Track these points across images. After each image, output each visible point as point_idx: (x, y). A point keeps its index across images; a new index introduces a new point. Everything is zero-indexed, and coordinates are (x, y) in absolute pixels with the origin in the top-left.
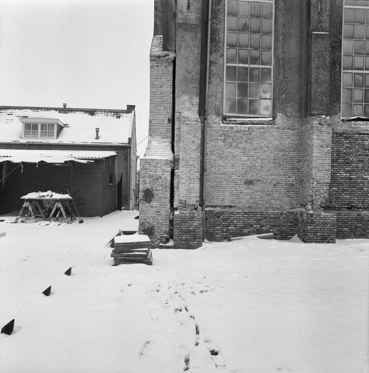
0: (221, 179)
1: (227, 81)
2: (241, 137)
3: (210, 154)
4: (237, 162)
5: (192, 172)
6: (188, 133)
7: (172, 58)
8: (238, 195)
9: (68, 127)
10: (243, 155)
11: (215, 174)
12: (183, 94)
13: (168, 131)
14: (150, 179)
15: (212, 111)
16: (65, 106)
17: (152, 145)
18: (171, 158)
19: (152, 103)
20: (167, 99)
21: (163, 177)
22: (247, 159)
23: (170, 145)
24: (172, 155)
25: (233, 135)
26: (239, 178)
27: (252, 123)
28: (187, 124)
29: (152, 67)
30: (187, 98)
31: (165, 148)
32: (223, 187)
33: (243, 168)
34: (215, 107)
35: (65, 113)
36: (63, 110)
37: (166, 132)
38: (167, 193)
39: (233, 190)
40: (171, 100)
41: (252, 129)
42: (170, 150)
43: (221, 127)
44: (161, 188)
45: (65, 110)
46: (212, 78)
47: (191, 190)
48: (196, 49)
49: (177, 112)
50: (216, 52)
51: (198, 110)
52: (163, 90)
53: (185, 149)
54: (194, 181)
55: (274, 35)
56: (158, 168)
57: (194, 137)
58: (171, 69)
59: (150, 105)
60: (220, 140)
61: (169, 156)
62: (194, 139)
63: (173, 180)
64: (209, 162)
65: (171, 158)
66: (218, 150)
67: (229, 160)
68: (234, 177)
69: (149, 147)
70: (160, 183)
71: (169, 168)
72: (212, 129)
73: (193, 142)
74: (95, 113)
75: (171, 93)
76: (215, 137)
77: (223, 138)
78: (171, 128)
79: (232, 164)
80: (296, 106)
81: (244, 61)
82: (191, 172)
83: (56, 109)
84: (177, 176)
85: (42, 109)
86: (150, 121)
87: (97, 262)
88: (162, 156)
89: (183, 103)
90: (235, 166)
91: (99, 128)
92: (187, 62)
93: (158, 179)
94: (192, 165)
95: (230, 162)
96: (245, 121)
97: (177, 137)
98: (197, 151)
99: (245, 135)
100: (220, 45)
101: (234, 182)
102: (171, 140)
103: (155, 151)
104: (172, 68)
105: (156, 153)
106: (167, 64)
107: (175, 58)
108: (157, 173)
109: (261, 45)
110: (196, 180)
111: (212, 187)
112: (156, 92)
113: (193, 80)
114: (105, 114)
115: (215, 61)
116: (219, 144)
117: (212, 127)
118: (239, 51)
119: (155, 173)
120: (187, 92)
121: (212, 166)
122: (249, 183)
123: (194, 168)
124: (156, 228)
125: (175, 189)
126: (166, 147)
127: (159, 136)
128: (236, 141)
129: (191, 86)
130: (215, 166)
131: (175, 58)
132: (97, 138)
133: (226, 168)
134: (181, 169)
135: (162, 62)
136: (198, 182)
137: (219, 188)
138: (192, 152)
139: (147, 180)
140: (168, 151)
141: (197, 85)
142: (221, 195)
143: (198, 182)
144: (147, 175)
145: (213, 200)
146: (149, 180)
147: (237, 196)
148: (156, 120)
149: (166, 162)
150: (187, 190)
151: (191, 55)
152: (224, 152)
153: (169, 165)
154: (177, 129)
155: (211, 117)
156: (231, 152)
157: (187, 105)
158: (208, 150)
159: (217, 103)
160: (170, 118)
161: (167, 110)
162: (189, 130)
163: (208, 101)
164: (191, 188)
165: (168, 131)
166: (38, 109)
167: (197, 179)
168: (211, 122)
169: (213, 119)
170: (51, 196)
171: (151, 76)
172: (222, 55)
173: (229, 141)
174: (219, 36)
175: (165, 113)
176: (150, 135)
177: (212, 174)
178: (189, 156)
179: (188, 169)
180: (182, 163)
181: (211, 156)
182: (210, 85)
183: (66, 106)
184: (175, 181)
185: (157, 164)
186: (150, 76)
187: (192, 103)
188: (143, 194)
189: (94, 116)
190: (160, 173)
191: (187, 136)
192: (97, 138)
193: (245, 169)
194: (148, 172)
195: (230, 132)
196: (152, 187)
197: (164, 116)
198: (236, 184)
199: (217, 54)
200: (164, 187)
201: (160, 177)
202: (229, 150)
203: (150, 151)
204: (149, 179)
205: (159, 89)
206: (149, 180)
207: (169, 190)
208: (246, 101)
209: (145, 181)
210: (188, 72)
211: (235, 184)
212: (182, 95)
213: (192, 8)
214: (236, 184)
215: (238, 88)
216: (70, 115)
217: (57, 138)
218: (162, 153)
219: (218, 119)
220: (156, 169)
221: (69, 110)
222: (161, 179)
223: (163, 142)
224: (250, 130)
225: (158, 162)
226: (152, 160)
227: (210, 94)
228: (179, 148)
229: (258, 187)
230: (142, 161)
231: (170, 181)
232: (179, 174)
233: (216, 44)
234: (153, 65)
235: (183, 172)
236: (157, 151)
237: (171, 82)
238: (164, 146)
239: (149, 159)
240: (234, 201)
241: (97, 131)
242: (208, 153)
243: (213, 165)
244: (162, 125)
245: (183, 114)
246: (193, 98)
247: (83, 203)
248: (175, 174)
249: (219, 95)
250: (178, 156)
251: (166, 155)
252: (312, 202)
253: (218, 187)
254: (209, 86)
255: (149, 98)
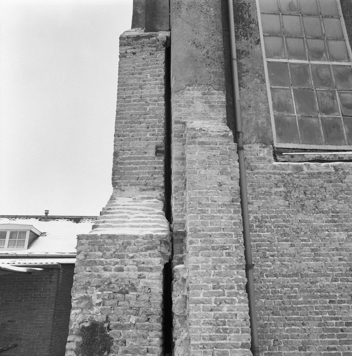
0: (292, 288)
1: (273, 87)
2: (322, 187)
3: (257, 226)
4: (325, 245)
5: (223, 266)
6: (207, 164)
7: (163, 38)
8: (342, 330)
9: (46, 235)
10: (335, 226)
11: (276, 276)
12: (189, 86)
13: (155, 173)
14: (102, 291)
15: (252, 135)
16: (47, 213)
17: (117, 205)
18: (163, 231)
19: (120, 118)
20: (154, 108)
21: (141, 284)
22: (346, 236)
23: (161, 204)
24: (165, 225)
25: (303, 183)
26: (336, 283)
27: (339, 158)
28: (202, 143)
29: (122, 56)
30: (197, 94)
31: (148, 210)
32: (300, 309)
33: (340, 259)
34: (257, 129)
35: (46, 221)
36: (44, 218)
37: (152, 175)
38: (152, 334)
39: (327, 318)
40: (162, 111)
41: (342, 169)
42: (163, 222)
43: (275, 167)
44: (133, 319)
45: (46, 218)
46: (243, 76)
47: (225, 325)
48: (212, 9)
49: (177, 122)
50: (246, 36)
51: (225, 116)
52: (145, 92)
53: (200, 203)
54: (230, 294)
55: (344, 17)
56: (126, 260)
57: (222, 173)
58: (161, 56)
59: (116, 123)
60: (275, 193)
61: (159, 227)
62: (222, 178)
63: (171, 293)
64: (257, 245)
65: (163, 231)
66: (276, 217)
67: (305, 240)
68: (324, 282)
69: (109, 209)
70: (132, 303)
71: (159, 259)
72: (256, 171)
73: (220, 185)
74: (81, 220)
75: (163, 98)
76: (263, 189)
77: (282, 189)
78: (162, 166)
79: (313, 250)
81: (301, 56)
82: (220, 267)
83: (36, 217)
84: (180, 281)
85: (20, 217)
86: (116, 154)
87: (259, 207)
88: (138, 227)
89: (190, 103)
90: (320, 255)
91: (48, 211)
92: (195, 29)
93: (127, 293)
94: (223, 248)
95: (307, 245)
96: (324, 156)
97: (177, 179)
98: (232, 210)
99: (331, 182)
100: (253, 26)
101: (327, 297)
102: (163, 195)
103: (122, 217)
104: (164, 54)
105: (124, 222)
106: (154, 49)
107: (169, 39)
108: (123, 274)
109: (324, 32)
110: (235, 290)
111: (271, 310)
112: (130, 97)
113: (209, 61)
114: (92, 222)
115: (245, 48)
116: (275, 204)
117: (256, 167)
118: (286, 42)
119: (117, 273)
120: (196, 82)
121: (265, 257)
123: (229, 254)
125: (176, 322)
126: (150, 208)
127: (134, 185)
128: (314, 196)
129: (205, 70)
130: (273, 256)
131: (169, 39)
133: (299, 261)
134: (191, 260)
135: (144, 45)
136: (242, 298)
137: (291, 312)
138: (219, 211)
139: (95, 295)
140: (156, 215)
141: (219, 68)
142: (296, 334)
143: (242, 298)
144: (95, 281)
145: (280, 348)
146: (98, 296)
147: (341, 333)
148: (130, 150)
149: (150, 244)
150: (211, 324)
151: (202, 19)
152: (288, 221)
153: (156, 251)
154: (177, 159)
155: (250, 147)
156: (306, 222)
157: (200, 107)
158: (252, 218)
159: (260, 121)
160: (161, 147)
161: (154, 130)
162: (208, 158)
163: (242, 119)
164: (225, 316)
165: (155, 173)
166: (16, 217)
167: (239, 287)
168: (251, 158)
169: (257, 152)
171: (120, 71)
172: (257, 41)
173: (297, 197)
174: (248, 14)
175: (148, 136)
176: (114, 184)
177: (267, 276)
178: (212, 224)
179: (210, 259)
180: (192, 244)
181: (259, 231)
182: (241, 88)
183: (48, 213)
184: (176, 298)
185: (125, 248)
186: (119, 70)
187: (209, 103)
188: (79, 339)
189: (79, 223)
190: (131, 273)
191: (203, 172)
193: (345, 261)
194: (97, 271)
195: (296, 178)
196: (107, 317)
197: (146, 143)
198: (330, 302)
199: (249, 40)
200: (143, 317)
201: (132, 285)
202: (300, 216)
203: (108, 218)
204: (100, 293)
205: (135, 91)
206: (98, 296)
207: (159, 325)
208: (314, 120)
209: (88, 298)
210: (197, 47)
211: (328, 300)
212: (187, 88)
214: (330, 302)
215: (295, 99)
216: (52, 222)
217: (29, 247)
218: (139, 221)
219: (266, 150)
220: (122, 262)
221: (51, 218)
222: (135, 290)
223: (143, 198)
224: (341, 172)
225: (126, 242)
226: (110, 237)
227: (244, 104)
228: (182, 205)
230: (83, 241)
231: (161, 298)
232: (185, 276)
233: (246, 25)
234: (125, 52)
235: (198, 267)
236: (126, 216)
237: (162, 77)
238: (147, 206)
239: (101, 235)
240: (335, 349)
242: (253, 225)
243: (268, 253)
244: (143, 161)
245: (189, 126)
246: (213, 94)
247: (16, 346)
248: (176, 275)
249: (262, 106)
250: (183, 224)
251: (151, 224)
253: (285, 309)
254: (240, 90)
255: (115, 108)
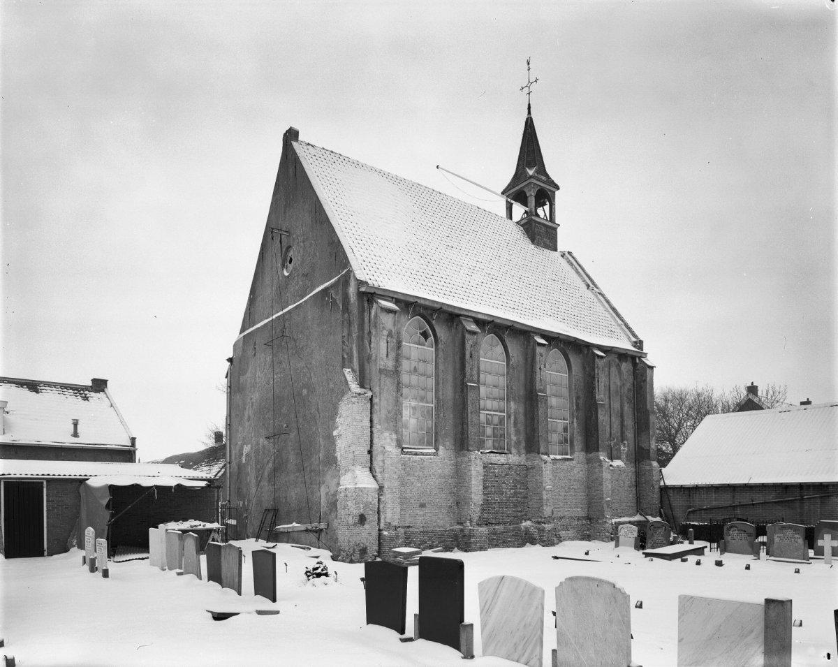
58: (369, 406)
80: (452, 441)
122: (422, 505)
124: (368, 548)
132: (75, 435)
157: (388, 440)
170: (204, 526)
192: (75, 435)
213: (390, 356)
229: (427, 510)
241: (76, 424)
252: (471, 520)
